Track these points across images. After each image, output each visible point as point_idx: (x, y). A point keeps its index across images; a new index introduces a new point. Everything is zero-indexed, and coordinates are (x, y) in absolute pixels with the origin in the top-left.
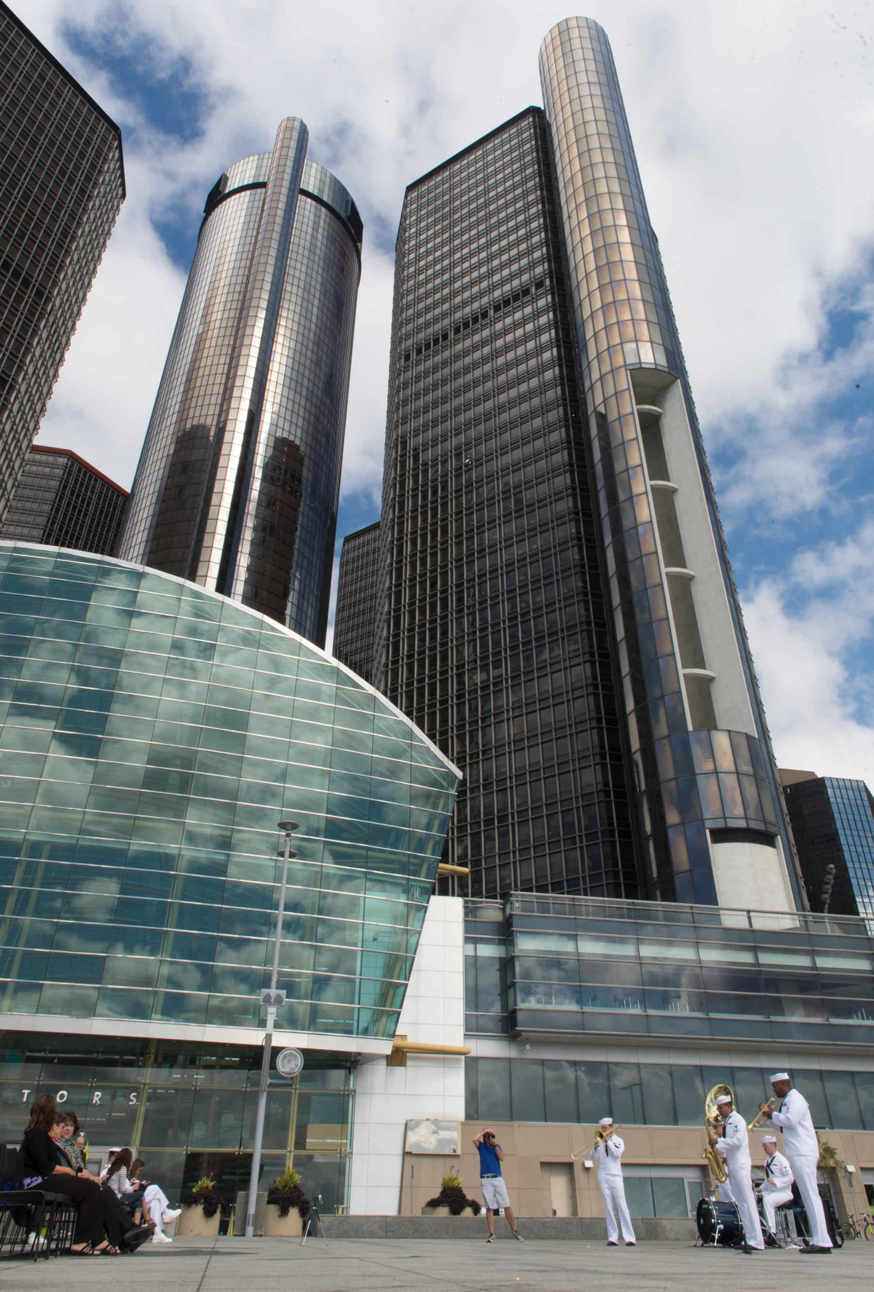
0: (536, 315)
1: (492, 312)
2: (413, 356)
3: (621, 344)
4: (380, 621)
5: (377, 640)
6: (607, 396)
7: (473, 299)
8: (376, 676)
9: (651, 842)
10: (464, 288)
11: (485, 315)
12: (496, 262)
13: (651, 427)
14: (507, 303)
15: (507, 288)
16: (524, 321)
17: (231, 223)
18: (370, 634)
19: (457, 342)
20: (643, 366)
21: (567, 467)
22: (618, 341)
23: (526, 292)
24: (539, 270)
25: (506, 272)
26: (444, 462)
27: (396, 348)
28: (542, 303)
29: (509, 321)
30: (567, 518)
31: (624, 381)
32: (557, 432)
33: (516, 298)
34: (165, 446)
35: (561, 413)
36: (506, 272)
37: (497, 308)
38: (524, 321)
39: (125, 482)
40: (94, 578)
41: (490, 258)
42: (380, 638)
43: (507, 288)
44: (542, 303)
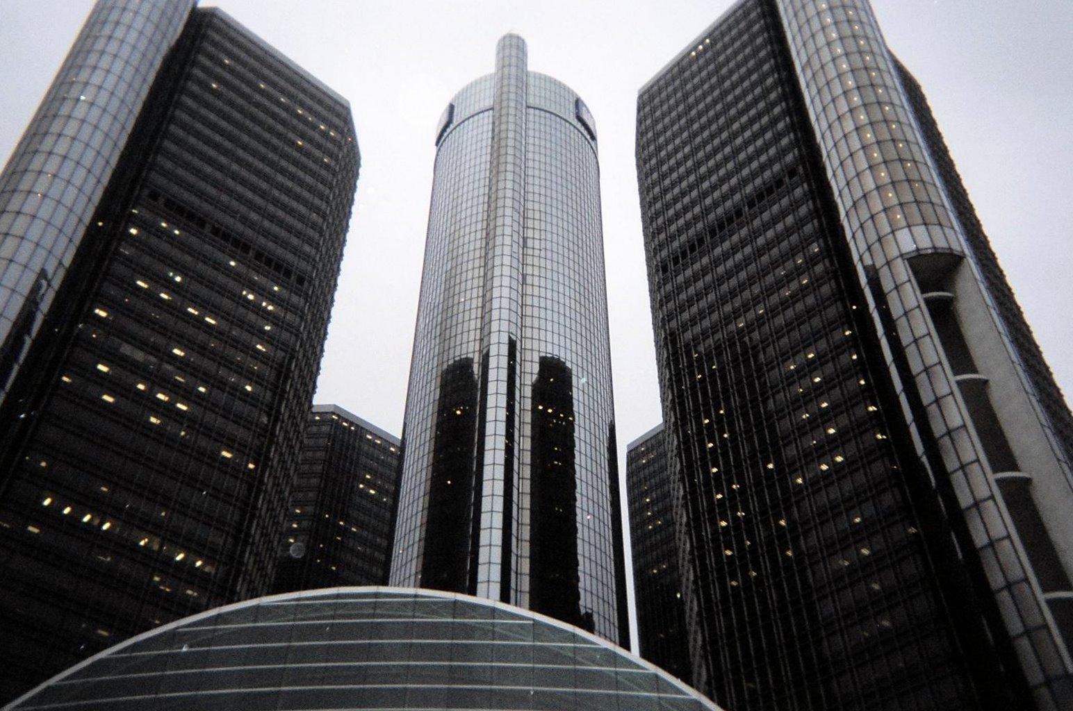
0: (795, 206)
1: (747, 209)
2: (671, 266)
3: (893, 232)
4: (677, 506)
5: (677, 527)
6: (842, 158)
7: (724, 198)
8: (683, 566)
9: (934, 485)
10: (714, 188)
11: (739, 213)
12: (730, 98)
13: (945, 317)
14: (760, 196)
15: (758, 181)
16: (783, 215)
17: (462, 168)
18: (667, 495)
19: (714, 247)
20: (921, 252)
21: (858, 368)
22: (888, 230)
23: (779, 183)
24: (789, 158)
25: (751, 149)
26: (719, 354)
27: (645, 198)
28: (798, 192)
29: (766, 216)
30: (853, 371)
31: (903, 272)
32: (834, 307)
33: (770, 191)
34: (432, 393)
35: (811, 206)
36: (751, 149)
37: (751, 205)
38: (783, 215)
39: (395, 430)
40: (372, 611)
41: (727, 108)
42: (681, 525)
43: (758, 181)
44: (798, 192)
